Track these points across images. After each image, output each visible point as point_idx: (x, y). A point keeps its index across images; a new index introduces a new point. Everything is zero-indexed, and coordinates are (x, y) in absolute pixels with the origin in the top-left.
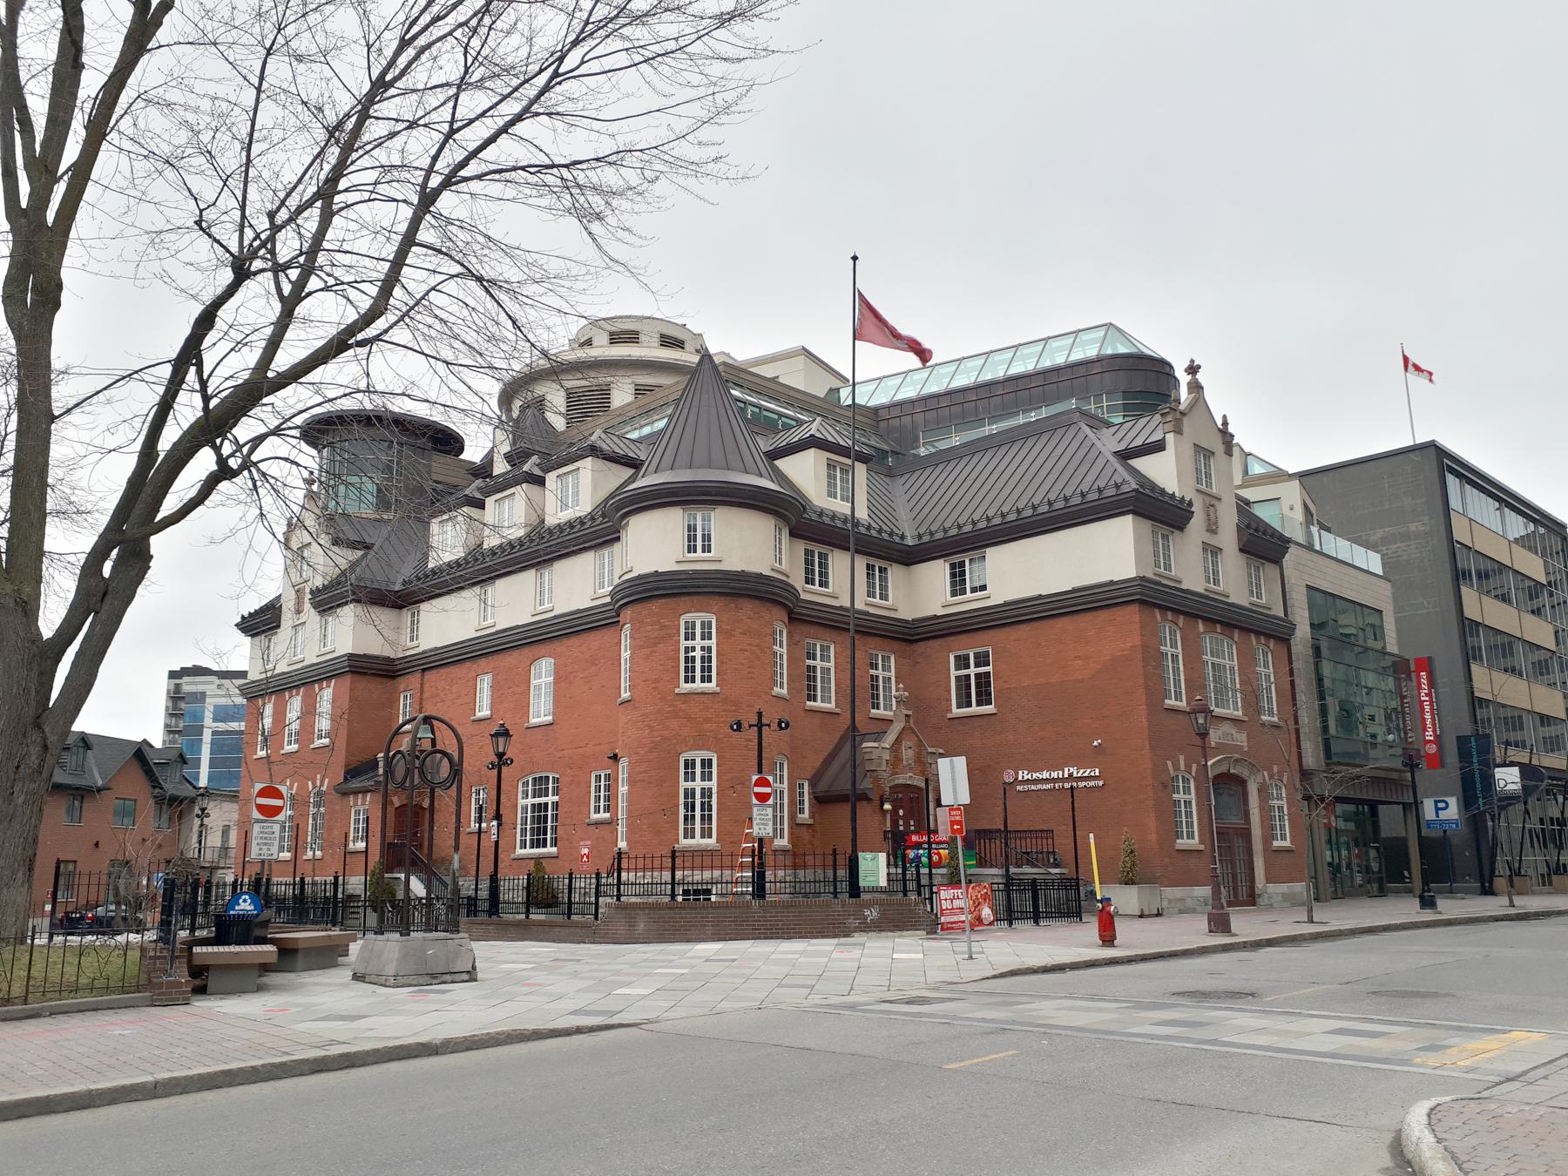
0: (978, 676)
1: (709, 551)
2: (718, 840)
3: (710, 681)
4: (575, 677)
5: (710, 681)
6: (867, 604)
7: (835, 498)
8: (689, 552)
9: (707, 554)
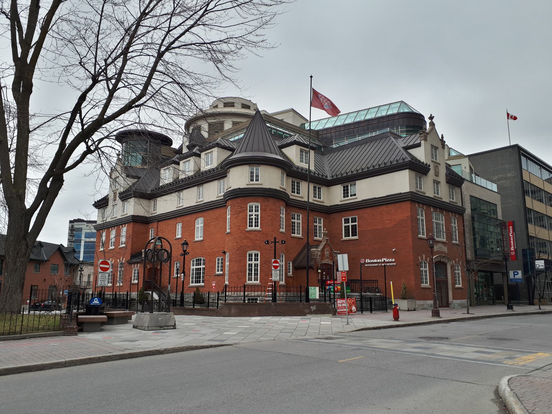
1: (258, 181)
3: (258, 226)
5: (258, 226)
7: (303, 162)
8: (251, 181)
9: (257, 182)
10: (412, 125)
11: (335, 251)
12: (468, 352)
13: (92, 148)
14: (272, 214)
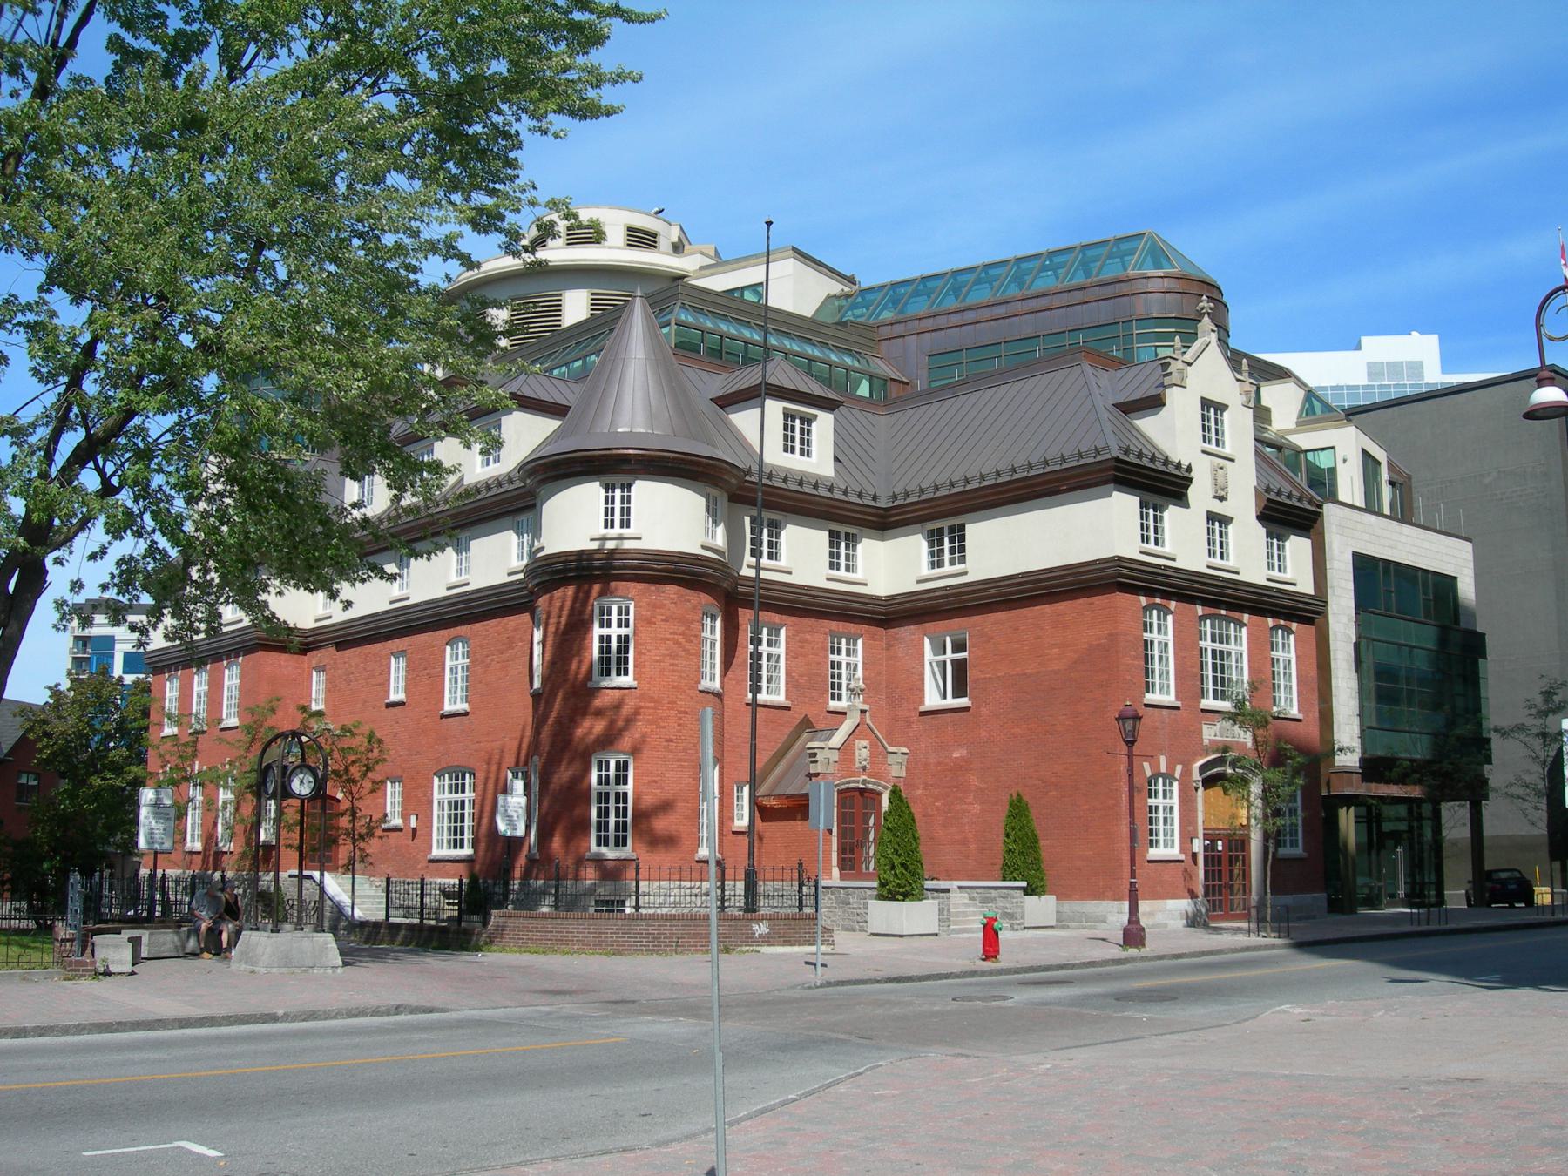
0: (954, 662)
1: (628, 526)
2: (1304, 850)
3: (626, 673)
4: (492, 660)
6: (828, 579)
7: (793, 451)
8: (606, 527)
10: (1173, 315)
11: (890, 749)
12: (545, 992)
13: (115, 481)
14: (671, 633)
